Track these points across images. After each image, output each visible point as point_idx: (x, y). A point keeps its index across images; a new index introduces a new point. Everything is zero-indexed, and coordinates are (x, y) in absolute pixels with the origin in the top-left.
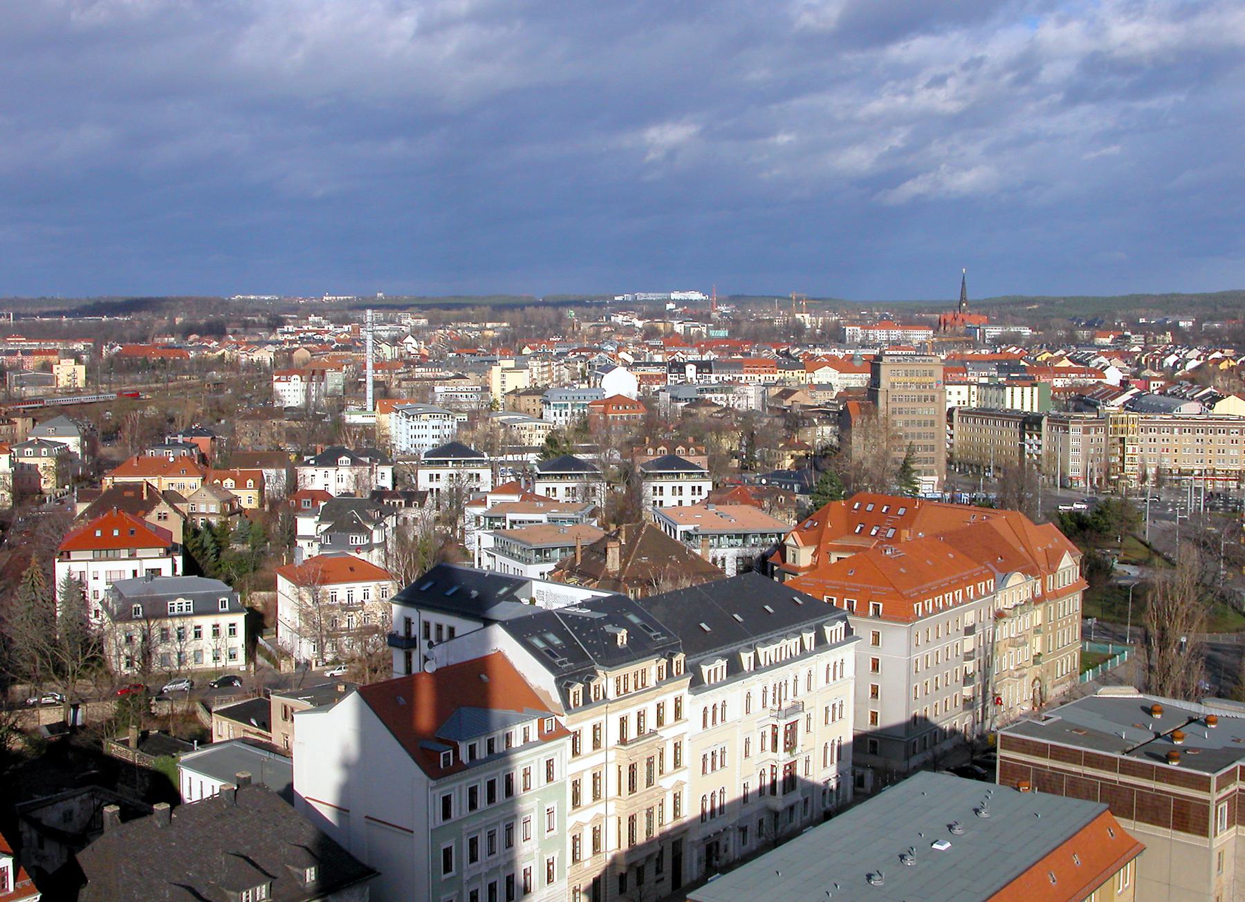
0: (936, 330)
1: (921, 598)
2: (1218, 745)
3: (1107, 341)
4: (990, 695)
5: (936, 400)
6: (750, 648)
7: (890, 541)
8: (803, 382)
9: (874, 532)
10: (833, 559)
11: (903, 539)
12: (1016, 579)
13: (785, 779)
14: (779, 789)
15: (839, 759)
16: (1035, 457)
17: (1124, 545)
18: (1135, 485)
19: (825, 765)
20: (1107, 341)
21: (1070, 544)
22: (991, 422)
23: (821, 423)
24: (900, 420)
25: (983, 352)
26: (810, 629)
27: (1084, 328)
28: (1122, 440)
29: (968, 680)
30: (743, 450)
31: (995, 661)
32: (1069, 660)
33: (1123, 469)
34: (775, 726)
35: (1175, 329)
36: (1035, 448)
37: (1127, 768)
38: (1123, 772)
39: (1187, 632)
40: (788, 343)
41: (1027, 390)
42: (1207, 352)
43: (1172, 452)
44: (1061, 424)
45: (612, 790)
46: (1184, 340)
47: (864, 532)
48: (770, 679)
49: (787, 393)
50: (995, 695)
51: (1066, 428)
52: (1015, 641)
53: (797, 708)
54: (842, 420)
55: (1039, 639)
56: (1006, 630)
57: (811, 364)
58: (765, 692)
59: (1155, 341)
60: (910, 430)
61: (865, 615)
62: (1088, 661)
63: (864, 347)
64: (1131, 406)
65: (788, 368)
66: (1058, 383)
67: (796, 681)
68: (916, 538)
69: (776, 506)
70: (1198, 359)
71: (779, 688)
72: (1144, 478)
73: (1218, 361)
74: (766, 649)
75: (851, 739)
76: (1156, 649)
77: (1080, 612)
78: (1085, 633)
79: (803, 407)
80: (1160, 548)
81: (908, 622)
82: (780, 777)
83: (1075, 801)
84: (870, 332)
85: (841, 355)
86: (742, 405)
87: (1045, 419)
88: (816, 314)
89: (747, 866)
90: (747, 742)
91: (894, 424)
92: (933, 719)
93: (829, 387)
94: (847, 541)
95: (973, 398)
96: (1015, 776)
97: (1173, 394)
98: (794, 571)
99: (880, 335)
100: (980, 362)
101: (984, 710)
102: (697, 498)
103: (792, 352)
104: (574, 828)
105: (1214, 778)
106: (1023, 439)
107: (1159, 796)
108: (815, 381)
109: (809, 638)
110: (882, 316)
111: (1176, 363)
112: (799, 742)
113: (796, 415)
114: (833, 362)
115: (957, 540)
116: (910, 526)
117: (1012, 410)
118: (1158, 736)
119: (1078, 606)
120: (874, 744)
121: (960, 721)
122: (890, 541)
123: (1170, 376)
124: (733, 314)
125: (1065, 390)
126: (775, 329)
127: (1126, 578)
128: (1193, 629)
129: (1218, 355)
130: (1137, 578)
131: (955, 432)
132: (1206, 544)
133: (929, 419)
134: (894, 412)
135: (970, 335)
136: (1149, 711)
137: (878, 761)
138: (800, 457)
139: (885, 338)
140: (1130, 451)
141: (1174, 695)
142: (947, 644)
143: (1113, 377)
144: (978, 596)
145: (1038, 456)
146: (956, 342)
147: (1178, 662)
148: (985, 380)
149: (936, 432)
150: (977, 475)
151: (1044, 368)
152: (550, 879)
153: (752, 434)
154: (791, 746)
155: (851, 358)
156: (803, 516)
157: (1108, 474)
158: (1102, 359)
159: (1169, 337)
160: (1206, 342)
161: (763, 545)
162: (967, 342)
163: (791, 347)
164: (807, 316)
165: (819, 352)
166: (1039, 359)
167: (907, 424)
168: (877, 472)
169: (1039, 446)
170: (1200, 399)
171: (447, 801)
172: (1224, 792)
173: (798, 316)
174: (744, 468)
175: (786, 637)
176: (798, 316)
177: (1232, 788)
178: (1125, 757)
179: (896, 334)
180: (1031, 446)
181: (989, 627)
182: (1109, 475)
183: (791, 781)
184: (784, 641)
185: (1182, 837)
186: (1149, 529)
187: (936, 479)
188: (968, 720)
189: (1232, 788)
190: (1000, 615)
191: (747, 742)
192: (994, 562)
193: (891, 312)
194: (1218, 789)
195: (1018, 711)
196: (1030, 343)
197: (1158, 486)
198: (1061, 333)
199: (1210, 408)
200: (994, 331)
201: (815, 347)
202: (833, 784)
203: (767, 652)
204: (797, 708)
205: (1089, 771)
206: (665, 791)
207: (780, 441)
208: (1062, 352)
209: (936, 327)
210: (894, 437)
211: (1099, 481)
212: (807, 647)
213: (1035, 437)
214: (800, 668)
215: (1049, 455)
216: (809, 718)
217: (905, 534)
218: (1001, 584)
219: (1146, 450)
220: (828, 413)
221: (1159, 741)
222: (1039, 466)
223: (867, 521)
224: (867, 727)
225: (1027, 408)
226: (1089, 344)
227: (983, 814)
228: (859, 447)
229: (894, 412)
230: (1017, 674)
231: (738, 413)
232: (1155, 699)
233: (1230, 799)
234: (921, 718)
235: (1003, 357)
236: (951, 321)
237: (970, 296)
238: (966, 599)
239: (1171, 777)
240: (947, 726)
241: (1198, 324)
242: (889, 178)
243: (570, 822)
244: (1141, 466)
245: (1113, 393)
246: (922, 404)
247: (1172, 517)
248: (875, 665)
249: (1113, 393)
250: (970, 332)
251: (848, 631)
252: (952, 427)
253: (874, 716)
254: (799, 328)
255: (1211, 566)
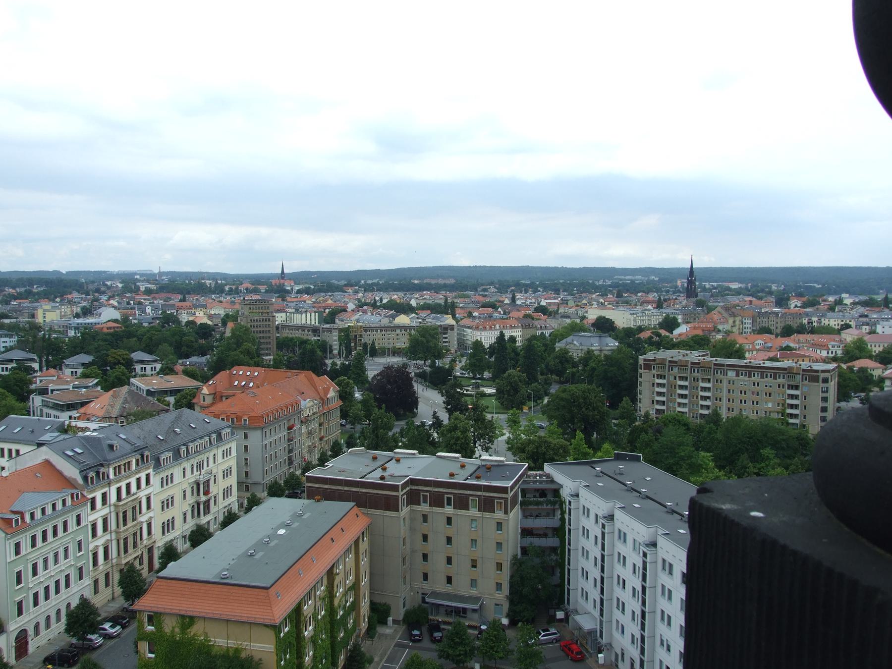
45: (114, 527)
89: (54, 463)
102: (154, 372)
104: (94, 549)
152: (81, 578)
171: (18, 546)
172: (405, 491)
185: (388, 513)
205: (346, 488)
206: (142, 522)
225: (313, 323)
243: (91, 547)
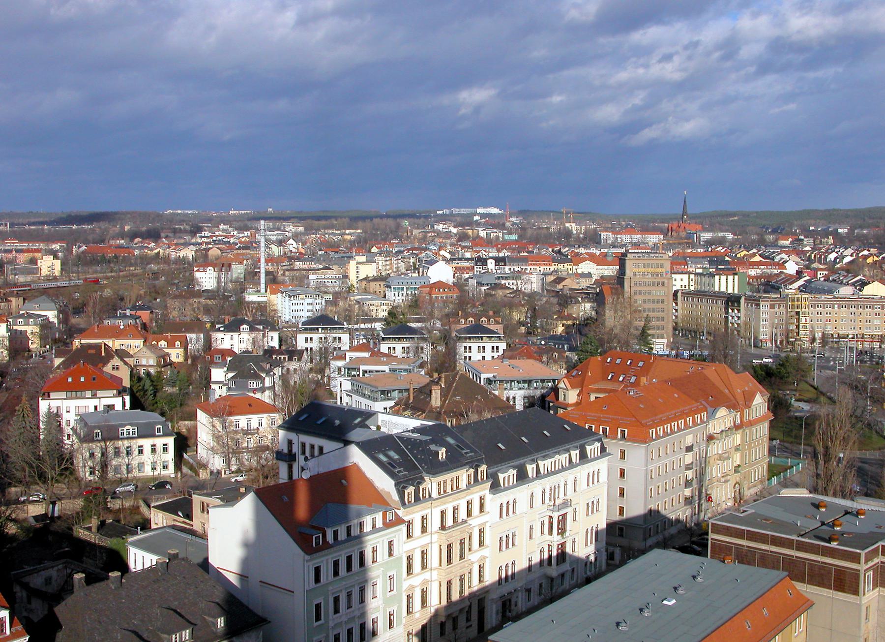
0: (666, 235)
1: (655, 425)
2: (866, 530)
3: (787, 243)
4: (704, 495)
5: (665, 285)
6: (533, 461)
7: (633, 385)
8: (571, 272)
9: (621, 379)
10: (592, 398)
11: (642, 384)
12: (722, 412)
13: (558, 554)
14: (554, 561)
15: (596, 540)
16: (736, 325)
17: (799, 388)
18: (807, 345)
19: (586, 545)
20: (787, 243)
21: (761, 387)
22: (704, 300)
23: (583, 301)
24: (639, 299)
25: (699, 250)
26: (576, 448)
27: (770, 233)
28: (798, 313)
29: (688, 484)
30: (528, 320)
31: (707, 471)
32: (760, 470)
33: (798, 334)
34: (551, 517)
35: (835, 234)
36: (736, 319)
37: (801, 547)
38: (798, 549)
39: (844, 450)
40: (560, 244)
41: (730, 278)
42: (858, 251)
43: (833, 321)
44: (754, 302)
46: (842, 242)
47: (614, 379)
48: (547, 483)
49: (559, 280)
50: (707, 495)
51: (758, 305)
52: (722, 456)
53: (566, 504)
54: (598, 299)
55: (738, 455)
56: (715, 449)
57: (577, 259)
58: (544, 492)
59: (821, 243)
60: (647, 306)
61: (615, 438)
62: (773, 471)
63: (614, 247)
64: (804, 289)
65: (560, 262)
66: (752, 272)
67: (566, 484)
68: (651, 383)
69: (551, 360)
70: (852, 255)
71: (554, 489)
72: (813, 340)
73: (865, 257)
74: (545, 462)
75: (605, 526)
76: (821, 462)
77: (767, 435)
78: (771, 451)
79: (571, 289)
80: (824, 390)
81: (646, 443)
82: (554, 553)
83: (764, 570)
84: (619, 236)
85: (597, 253)
86: (527, 288)
87: (743, 298)
88: (580, 224)
90: (531, 528)
91: (636, 301)
92: (663, 512)
93: (589, 275)
94: (602, 385)
95: (692, 283)
96: (722, 552)
97: (834, 280)
98: (565, 407)
99: (626, 238)
100: (696, 258)
101: (700, 505)
103: (563, 250)
105: (863, 553)
106: (727, 313)
107: (824, 566)
108: (580, 272)
109: (575, 454)
110: (627, 225)
111: (836, 258)
112: (568, 528)
113: (566, 296)
114: (592, 258)
115: (680, 384)
116: (647, 374)
117: (719, 292)
118: (823, 524)
119: (766, 431)
120: (621, 530)
121: (682, 513)
122: (633, 385)
123: (831, 268)
124: (521, 223)
125: (757, 277)
126: (551, 234)
127: (800, 411)
128: (848, 447)
129: (865, 253)
130: (808, 411)
131: (679, 308)
132: (857, 388)
133: (660, 298)
134: (635, 294)
135: (689, 238)
136: (817, 506)
137: (624, 542)
138: (569, 325)
139: (629, 240)
140: (803, 321)
141: (835, 495)
142: (673, 458)
143: (791, 268)
144: (695, 424)
145: (738, 324)
146: (680, 244)
147: (838, 471)
148: (700, 271)
149: (665, 307)
150: (695, 338)
151: (742, 262)
153: (535, 309)
154: (562, 531)
155: (605, 255)
156: (571, 367)
157: (787, 337)
158: (784, 256)
159: (831, 240)
160: (857, 243)
161: (543, 388)
162: (687, 243)
163: (562, 247)
164: (574, 225)
165: (582, 250)
166: (738, 256)
167: (644, 302)
168: (623, 336)
169: (739, 318)
170: (853, 284)
172: (870, 564)
173: (567, 225)
174: (529, 333)
175: (559, 453)
176: (567, 225)
177: (876, 561)
178: (800, 539)
179: (637, 238)
180: (733, 317)
181: (703, 446)
182: (788, 338)
183: (562, 556)
184: (557, 456)
186: (816, 376)
187: (665, 341)
188: (688, 512)
189: (876, 561)
190: (710, 438)
191: (531, 528)
192: (707, 400)
193: (634, 222)
194: (866, 562)
195: (724, 506)
196: (732, 244)
197: (823, 346)
198: (754, 237)
199: (860, 290)
200: (706, 236)
201: (579, 247)
202: (592, 558)
203: (545, 464)
204: (566, 504)
205: (774, 549)
207: (555, 314)
208: (755, 250)
209: (665, 233)
210: (635, 311)
211: (781, 342)
212: (574, 461)
213: (736, 311)
214: (569, 476)
215: (746, 324)
216: (575, 511)
217: (644, 380)
218: (711, 416)
219: (815, 321)
220: (588, 294)
221: (824, 527)
222: (738, 331)
223: (617, 370)
224: (617, 517)
225: (730, 291)
226: (774, 245)
227: (699, 579)
228: (611, 318)
229: (635, 294)
230: (723, 480)
231: (524, 294)
232: (821, 497)
233: (874, 568)
234: (655, 511)
235: (713, 254)
236: (676, 229)
237: (690, 211)
238: (687, 427)
239: (832, 553)
240: (673, 517)
241: (851, 230)
242: (632, 127)
244: (811, 332)
245: (791, 279)
246: (656, 287)
247: (833, 368)
248: (622, 473)
249: (791, 279)
250: (689, 236)
251: (603, 449)
252: (677, 304)
253: (621, 510)
254: (568, 234)
255: (861, 403)
